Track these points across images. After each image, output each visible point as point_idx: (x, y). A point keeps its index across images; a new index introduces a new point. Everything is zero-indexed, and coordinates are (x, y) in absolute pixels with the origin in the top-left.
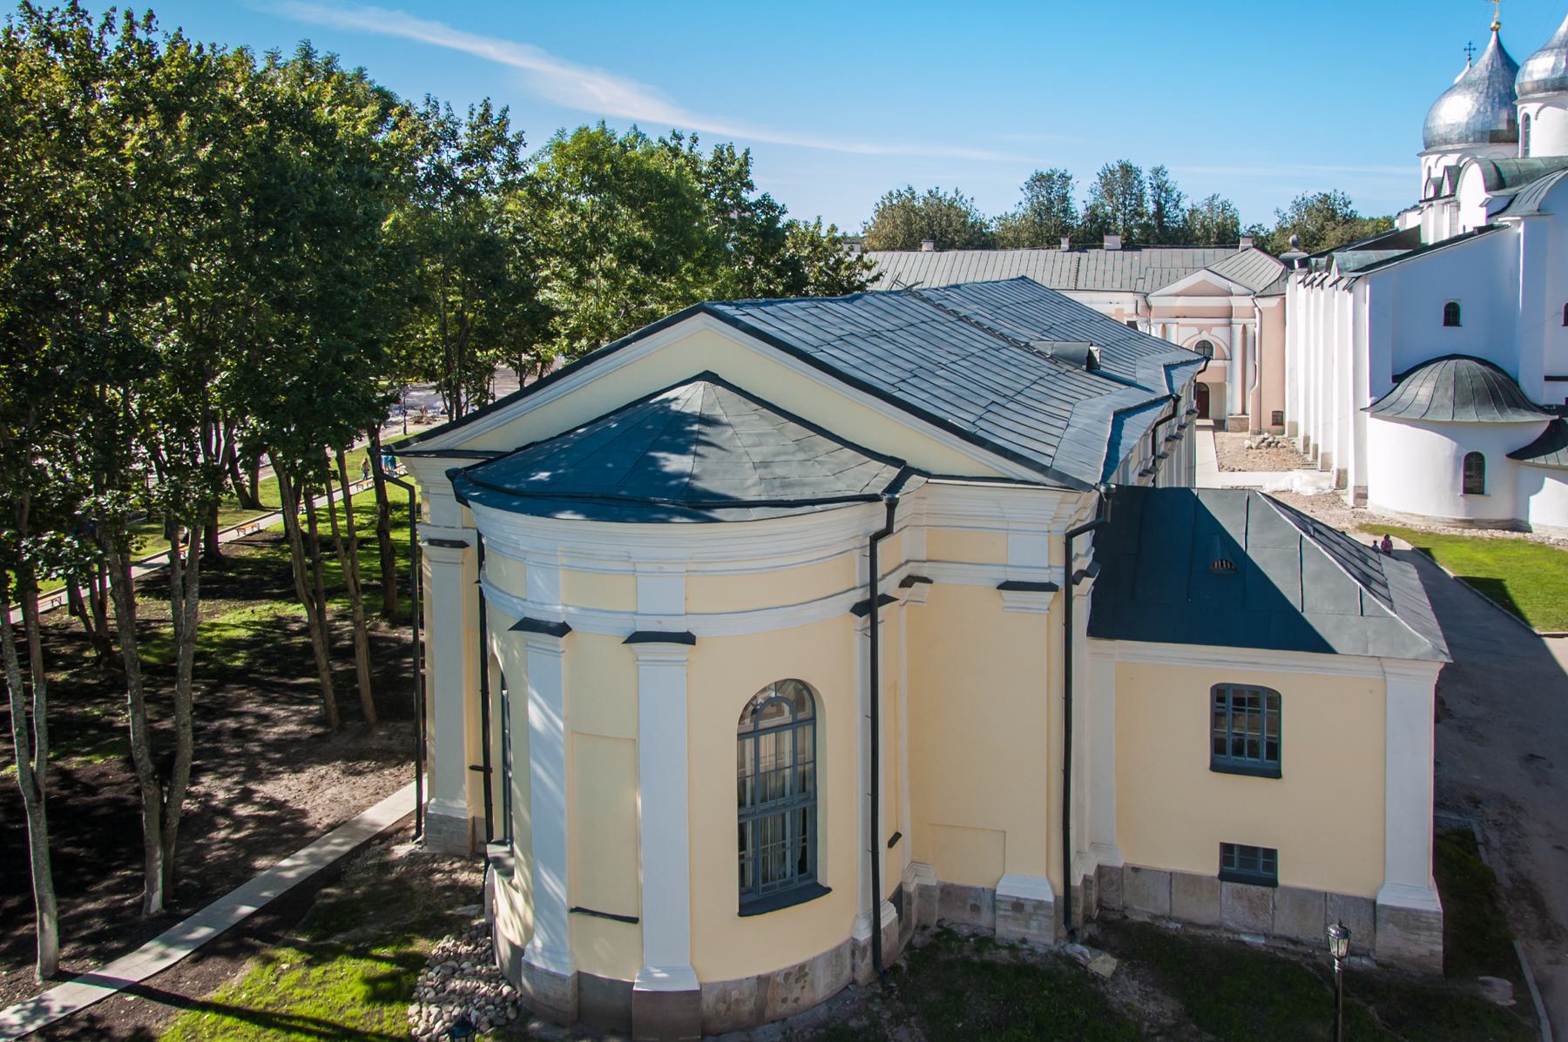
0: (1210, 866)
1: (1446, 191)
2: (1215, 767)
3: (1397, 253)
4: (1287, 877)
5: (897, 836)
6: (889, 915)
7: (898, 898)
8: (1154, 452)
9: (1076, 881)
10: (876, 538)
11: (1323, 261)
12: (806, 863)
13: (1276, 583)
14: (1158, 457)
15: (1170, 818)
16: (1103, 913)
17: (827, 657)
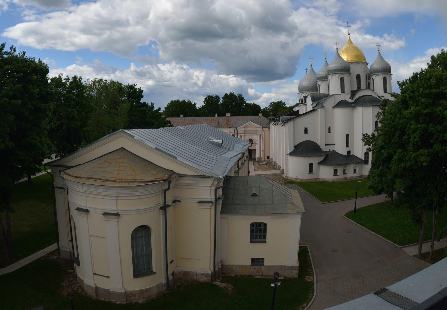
0: (249, 263)
1: (304, 102)
2: (251, 242)
3: (294, 116)
4: (266, 263)
5: (172, 261)
6: (171, 277)
7: (173, 274)
8: (238, 167)
9: (217, 269)
10: (165, 191)
11: (278, 118)
12: (150, 268)
13: (427, 298)
14: (239, 169)
15: (241, 253)
16: (222, 272)
17: (154, 221)
